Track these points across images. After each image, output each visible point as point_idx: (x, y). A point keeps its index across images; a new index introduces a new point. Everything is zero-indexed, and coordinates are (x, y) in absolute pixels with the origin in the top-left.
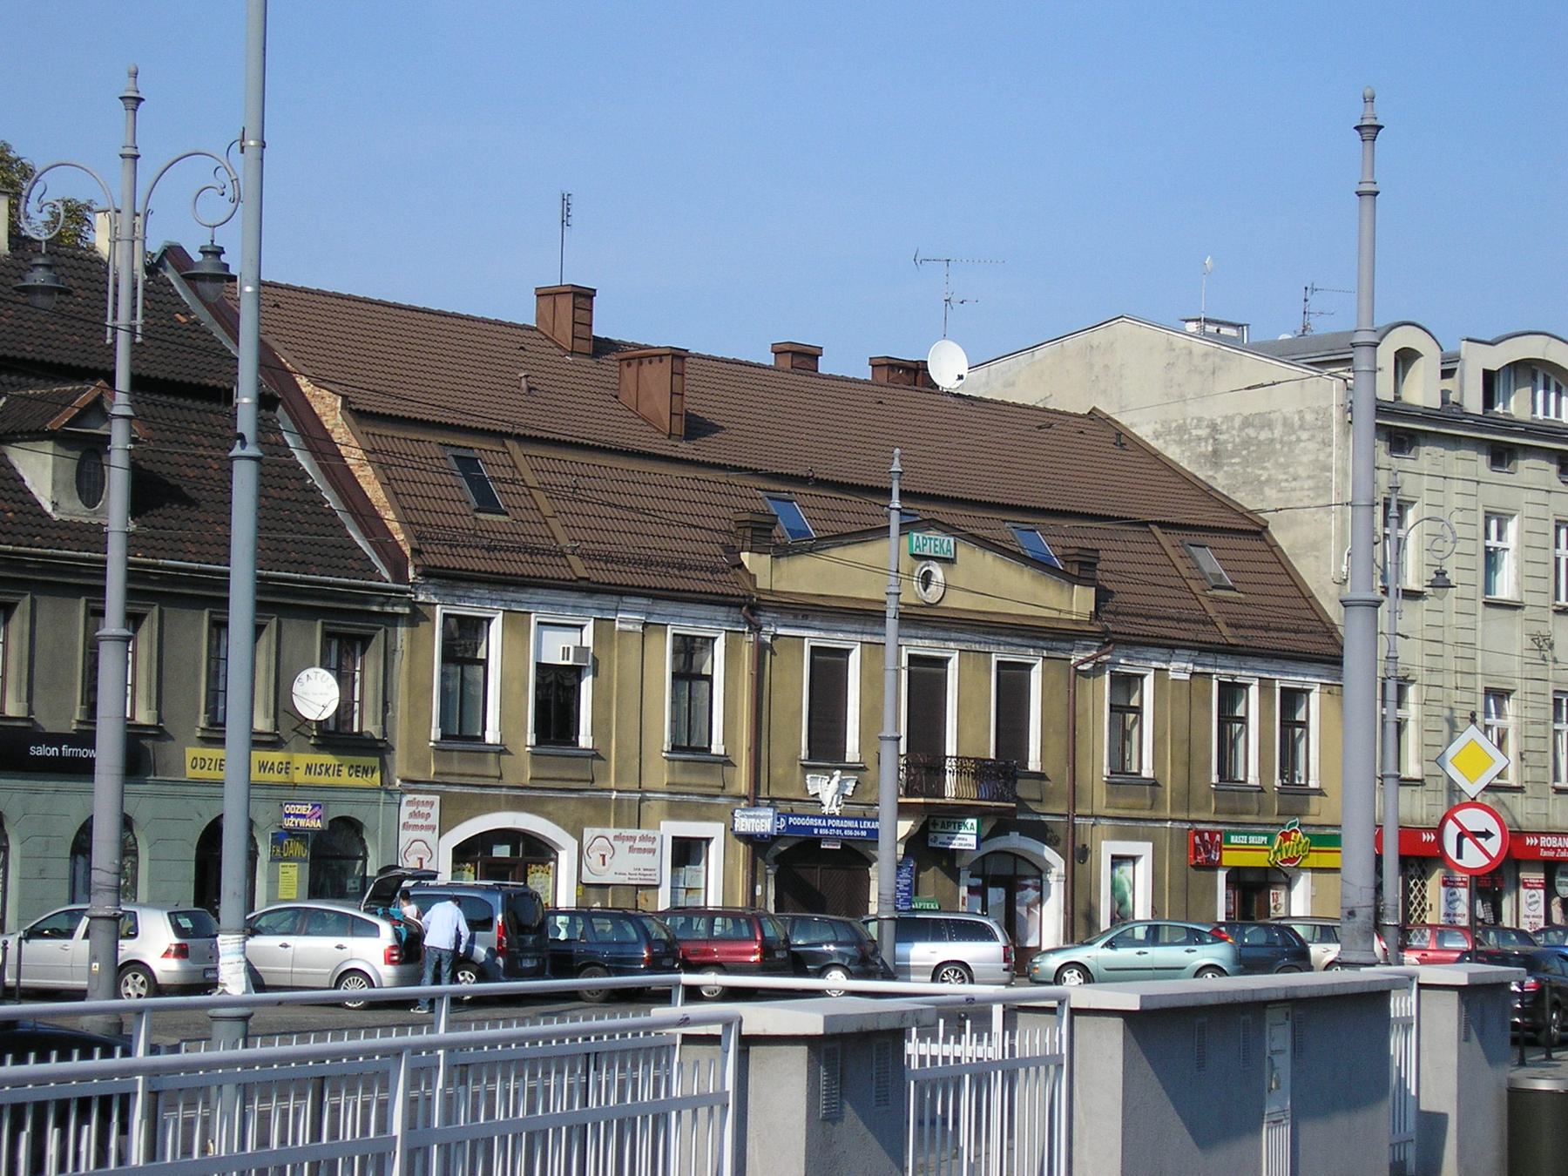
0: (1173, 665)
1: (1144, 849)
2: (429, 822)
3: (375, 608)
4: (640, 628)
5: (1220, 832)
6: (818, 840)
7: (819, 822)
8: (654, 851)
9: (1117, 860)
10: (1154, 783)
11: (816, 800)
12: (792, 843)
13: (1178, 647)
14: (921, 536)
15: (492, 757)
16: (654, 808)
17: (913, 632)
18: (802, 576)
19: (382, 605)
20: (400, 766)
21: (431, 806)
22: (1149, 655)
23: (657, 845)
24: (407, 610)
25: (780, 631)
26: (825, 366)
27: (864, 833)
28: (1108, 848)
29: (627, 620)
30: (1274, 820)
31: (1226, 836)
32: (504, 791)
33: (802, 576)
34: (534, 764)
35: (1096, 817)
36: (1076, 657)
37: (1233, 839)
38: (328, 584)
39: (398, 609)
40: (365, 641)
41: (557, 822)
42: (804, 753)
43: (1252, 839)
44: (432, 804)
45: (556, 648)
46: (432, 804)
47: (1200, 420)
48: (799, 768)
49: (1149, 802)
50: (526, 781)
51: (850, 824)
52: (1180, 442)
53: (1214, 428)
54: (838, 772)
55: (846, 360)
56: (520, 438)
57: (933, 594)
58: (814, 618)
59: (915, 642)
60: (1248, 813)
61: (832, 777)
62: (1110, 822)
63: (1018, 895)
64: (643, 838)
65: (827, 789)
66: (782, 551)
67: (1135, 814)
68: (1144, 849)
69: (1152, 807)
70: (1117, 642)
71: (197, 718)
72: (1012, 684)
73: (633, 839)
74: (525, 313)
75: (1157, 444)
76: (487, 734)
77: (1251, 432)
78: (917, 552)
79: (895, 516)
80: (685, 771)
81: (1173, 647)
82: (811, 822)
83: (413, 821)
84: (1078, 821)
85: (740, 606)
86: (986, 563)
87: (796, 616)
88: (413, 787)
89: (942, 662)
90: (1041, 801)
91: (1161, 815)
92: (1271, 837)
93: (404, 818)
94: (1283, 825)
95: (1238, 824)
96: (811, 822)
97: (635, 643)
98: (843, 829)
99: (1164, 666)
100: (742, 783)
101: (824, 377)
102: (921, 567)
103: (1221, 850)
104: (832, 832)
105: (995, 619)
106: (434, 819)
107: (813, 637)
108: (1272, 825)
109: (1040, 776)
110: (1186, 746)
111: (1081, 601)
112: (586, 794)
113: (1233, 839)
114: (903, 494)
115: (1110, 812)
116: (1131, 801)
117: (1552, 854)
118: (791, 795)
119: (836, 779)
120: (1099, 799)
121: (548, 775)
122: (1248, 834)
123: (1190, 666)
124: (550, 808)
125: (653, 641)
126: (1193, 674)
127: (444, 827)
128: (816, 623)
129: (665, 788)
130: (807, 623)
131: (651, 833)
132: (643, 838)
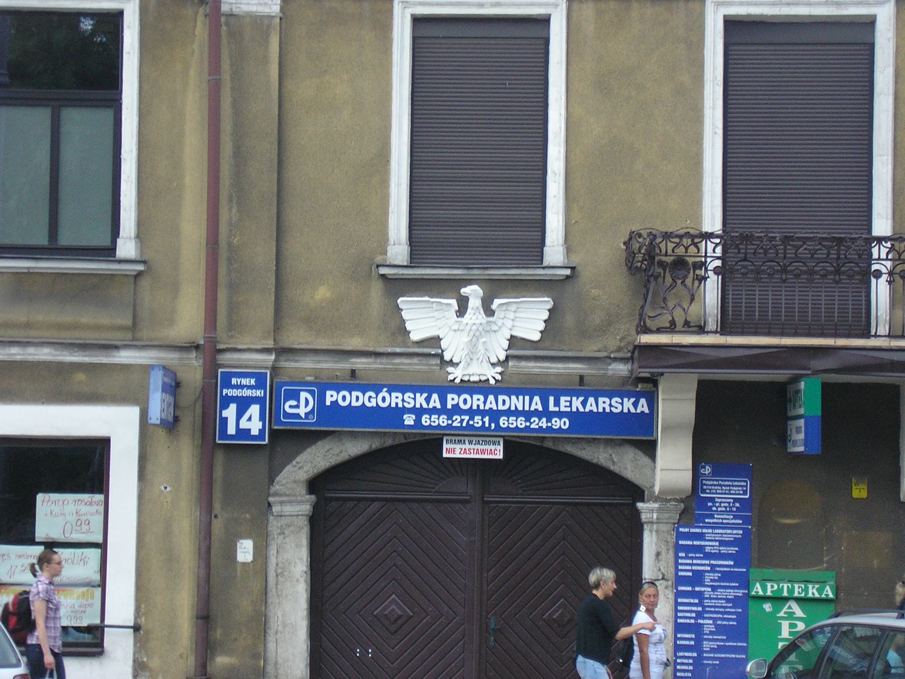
6: (430, 443)
27: (557, 423)
48: (376, 290)
51: (517, 402)
65: (473, 336)
82: (395, 399)
96: (395, 399)
98: (495, 415)
104: (457, 421)
117: (521, 423)
118: (355, 343)
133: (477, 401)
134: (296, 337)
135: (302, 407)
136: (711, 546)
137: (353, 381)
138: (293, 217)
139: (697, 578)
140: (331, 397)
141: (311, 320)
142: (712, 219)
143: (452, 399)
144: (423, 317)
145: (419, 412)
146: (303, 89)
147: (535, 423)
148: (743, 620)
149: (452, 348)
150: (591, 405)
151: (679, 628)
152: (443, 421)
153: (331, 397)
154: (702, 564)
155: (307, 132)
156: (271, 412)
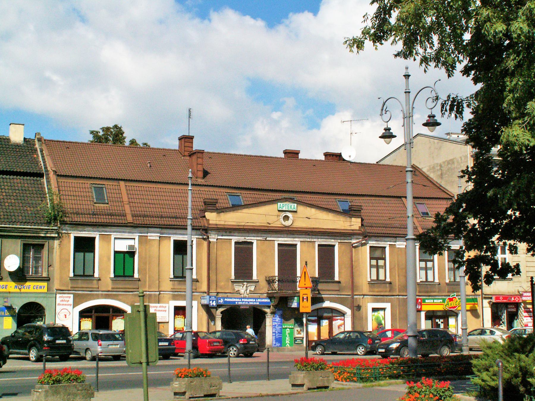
0: (398, 243)
1: (388, 306)
2: (69, 303)
3: (43, 235)
4: (158, 238)
5: (421, 299)
7: (238, 300)
8: (166, 311)
9: (374, 310)
10: (390, 283)
11: (238, 292)
12: (228, 307)
13: (399, 237)
14: (281, 204)
15: (95, 282)
16: (166, 295)
17: (279, 236)
18: (231, 218)
19: (46, 234)
20: (56, 285)
21: (70, 298)
22: (386, 240)
23: (167, 309)
24: (56, 235)
25: (219, 237)
26: (301, 156)
27: (258, 303)
28: (371, 305)
29: (153, 236)
30: (447, 294)
31: (424, 300)
32: (100, 293)
33: (231, 218)
34: (113, 283)
35: (364, 295)
36: (354, 241)
37: (427, 301)
38: (7, 228)
39: (53, 235)
40: (42, 246)
41: (124, 302)
42: (233, 277)
43: (435, 301)
44: (70, 297)
45: (122, 246)
46: (70, 297)
47: (437, 164)
48: (230, 282)
49: (388, 289)
50: (110, 289)
52: (434, 172)
53: (441, 166)
54: (245, 283)
55: (124, 135)
56: (124, 180)
57: (288, 223)
58: (234, 233)
59: (280, 239)
60: (434, 292)
61: (244, 285)
62: (371, 297)
63: (334, 322)
64: (160, 307)
66: (220, 210)
67: (382, 294)
68: (388, 306)
69: (390, 291)
70: (370, 237)
71: (110, 273)
72: (326, 253)
73: (157, 307)
74: (375, 163)
75: (428, 173)
76: (95, 274)
77: (449, 166)
78: (280, 209)
79: (190, 192)
80: (179, 284)
81: (396, 237)
83: (61, 303)
84: (355, 297)
85: (199, 229)
86: (312, 212)
87: (226, 232)
88: (61, 292)
89: (333, 246)
90: (339, 290)
91: (394, 294)
92: (444, 301)
93: (58, 301)
94: (449, 296)
95: (429, 296)
96: (234, 300)
97: (156, 244)
98: (249, 302)
99: (393, 243)
100: (204, 288)
101: (301, 159)
102: (284, 214)
103: (421, 305)
105: (342, 231)
106: (71, 301)
107: (235, 239)
108: (445, 296)
109: (339, 282)
110: (404, 271)
111: (355, 224)
112: (135, 293)
113: (427, 301)
114: (188, 184)
115: (371, 293)
116: (380, 289)
118: (227, 291)
119: (245, 285)
120: (365, 289)
121: (119, 287)
122: (433, 299)
123: (159, 234)
124: (121, 297)
125: (164, 243)
126: (217, 239)
127: (75, 305)
128: (236, 234)
129: (169, 290)
130: (232, 234)
131: (164, 305)
132: (160, 307)
133: (246, 300)
134: (219, 291)
135: (221, 301)
136: (277, 321)
137: (227, 298)
138: (218, 272)
139: (275, 325)
140: (225, 299)
141: (221, 288)
142: (277, 274)
143: (243, 300)
144: (237, 287)
145: (238, 302)
146: (219, 253)
147: (255, 303)
148: (281, 331)
149: (242, 291)
150: (262, 300)
151: (273, 333)
152: (241, 303)
153: (225, 299)
154: (276, 323)
155: (220, 259)
156: (217, 302)
